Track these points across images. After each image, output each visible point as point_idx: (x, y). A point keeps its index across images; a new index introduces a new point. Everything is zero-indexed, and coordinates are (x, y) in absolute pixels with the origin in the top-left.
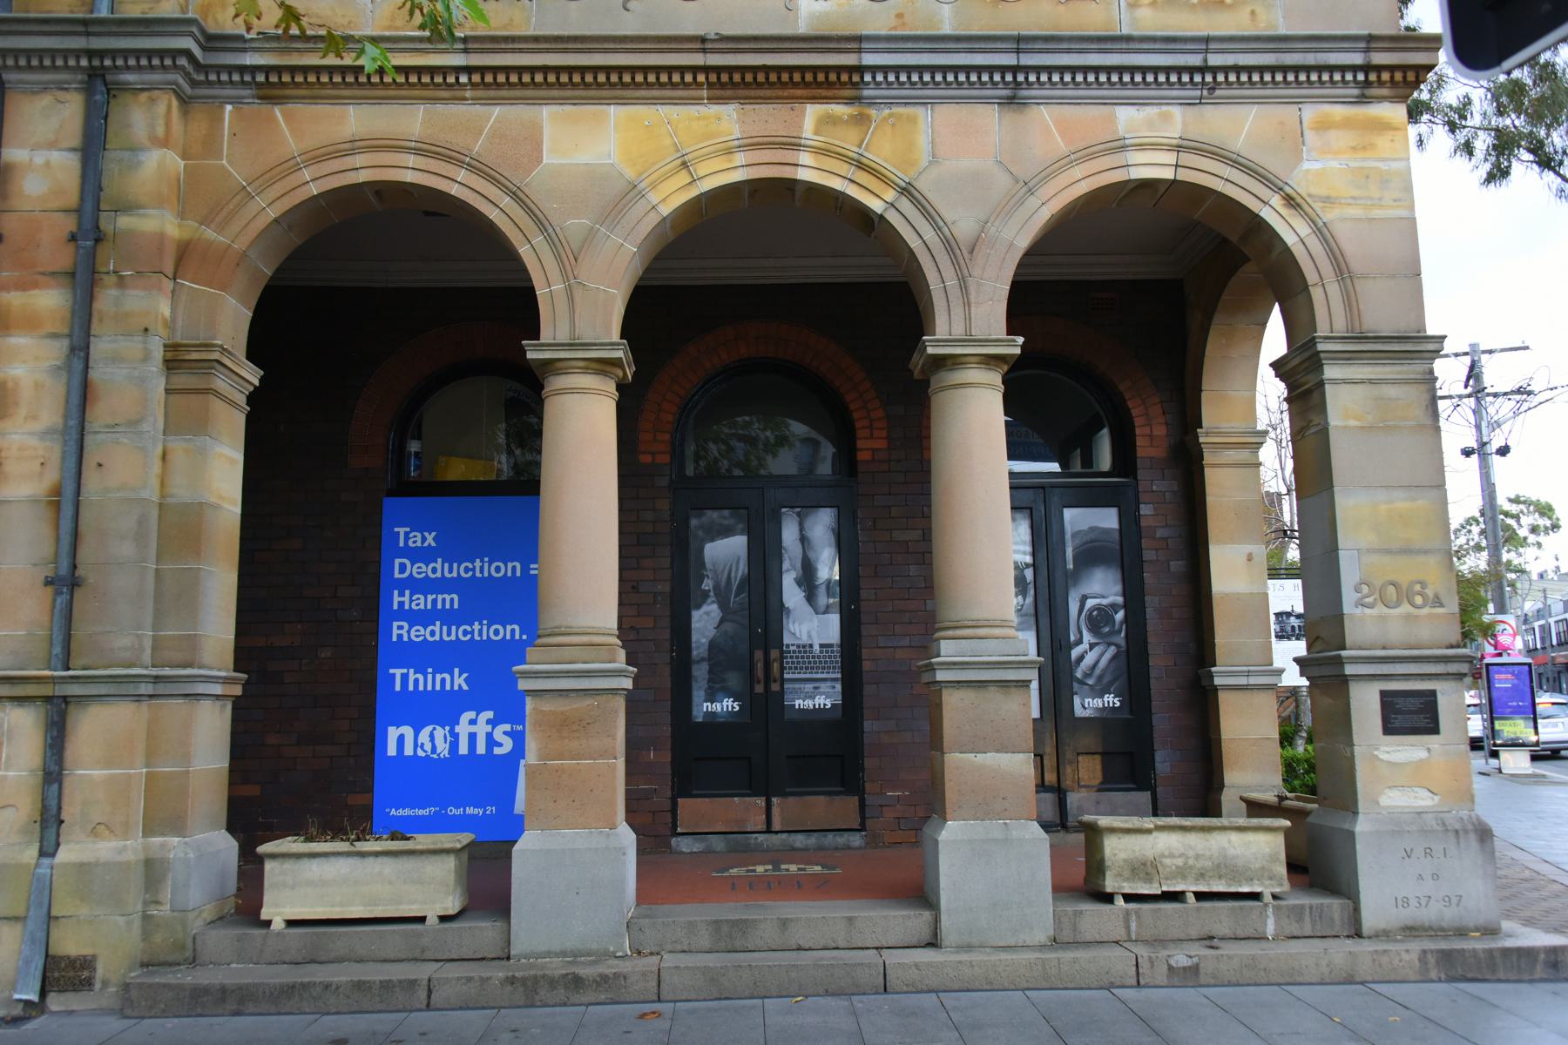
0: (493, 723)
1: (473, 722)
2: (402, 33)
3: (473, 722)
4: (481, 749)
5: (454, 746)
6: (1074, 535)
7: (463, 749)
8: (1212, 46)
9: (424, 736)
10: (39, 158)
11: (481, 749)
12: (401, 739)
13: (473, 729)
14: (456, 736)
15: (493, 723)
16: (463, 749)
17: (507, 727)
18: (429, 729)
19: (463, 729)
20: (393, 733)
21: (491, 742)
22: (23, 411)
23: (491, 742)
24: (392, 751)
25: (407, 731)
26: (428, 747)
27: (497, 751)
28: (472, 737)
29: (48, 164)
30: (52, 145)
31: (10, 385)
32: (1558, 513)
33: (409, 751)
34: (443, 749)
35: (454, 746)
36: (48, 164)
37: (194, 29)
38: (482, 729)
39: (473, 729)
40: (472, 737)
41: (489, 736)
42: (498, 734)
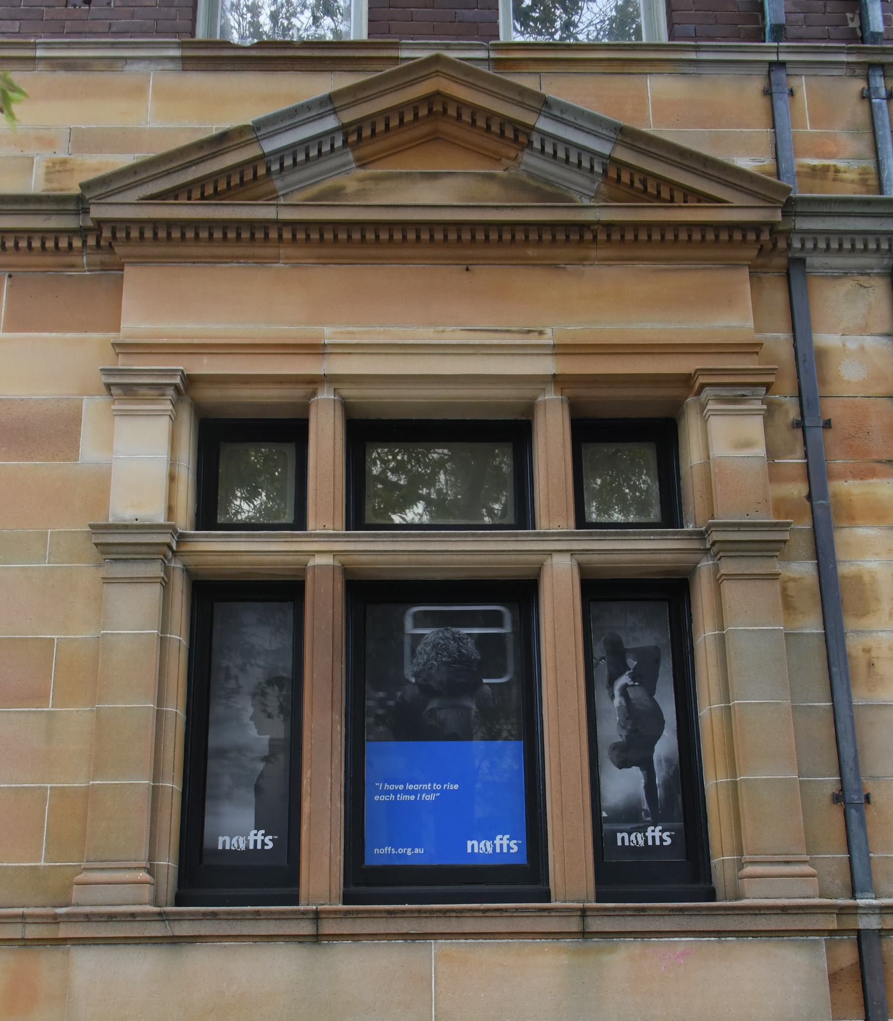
1: (501, 839)
4: (259, 847)
6: (660, 761)
7: (498, 850)
9: (234, 841)
10: (852, 343)
11: (259, 847)
12: (473, 846)
13: (501, 842)
14: (495, 845)
15: (264, 835)
17: (271, 837)
18: (236, 838)
19: (497, 842)
21: (509, 847)
22: (885, 606)
23: (509, 847)
25: (475, 842)
26: (484, 849)
27: (511, 851)
29: (862, 348)
30: (863, 330)
31: (866, 579)
33: (476, 851)
35: (494, 849)
36: (862, 348)
39: (501, 842)
40: (501, 845)
41: (263, 841)
42: (267, 840)
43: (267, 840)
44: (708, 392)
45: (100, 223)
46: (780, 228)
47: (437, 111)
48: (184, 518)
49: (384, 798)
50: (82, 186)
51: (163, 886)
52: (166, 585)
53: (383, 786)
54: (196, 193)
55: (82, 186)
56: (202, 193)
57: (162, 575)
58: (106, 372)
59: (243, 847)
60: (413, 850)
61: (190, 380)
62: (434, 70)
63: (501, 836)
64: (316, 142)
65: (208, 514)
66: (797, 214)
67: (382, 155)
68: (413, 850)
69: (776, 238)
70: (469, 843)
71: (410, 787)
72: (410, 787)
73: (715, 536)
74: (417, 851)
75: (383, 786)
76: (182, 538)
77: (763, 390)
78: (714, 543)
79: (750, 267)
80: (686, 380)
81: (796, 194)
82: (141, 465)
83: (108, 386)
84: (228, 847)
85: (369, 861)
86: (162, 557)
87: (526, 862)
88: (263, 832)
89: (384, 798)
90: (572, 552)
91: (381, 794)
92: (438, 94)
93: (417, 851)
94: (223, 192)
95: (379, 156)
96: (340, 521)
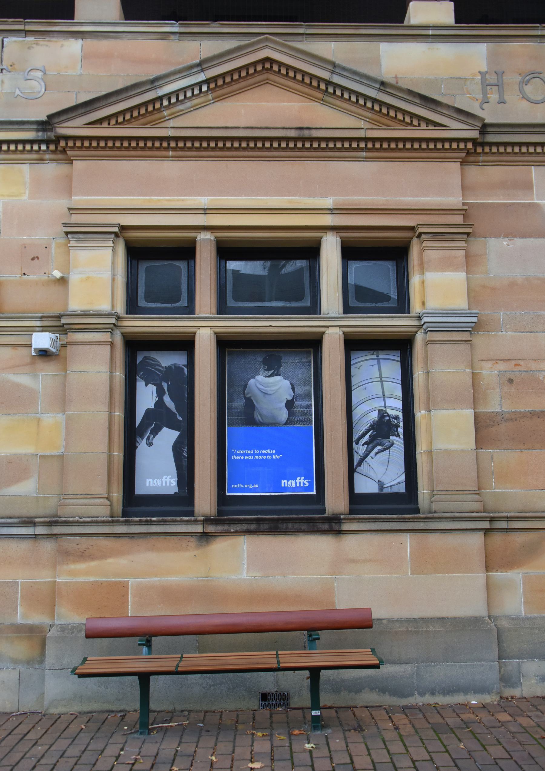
0: (171, 478)
1: (166, 478)
2: (9, 315)
3: (166, 478)
4: (168, 485)
5: (162, 484)
7: (164, 484)
8: (337, 70)
11: (168, 485)
12: (150, 482)
15: (171, 478)
16: (164, 484)
19: (298, 481)
20: (148, 481)
21: (304, 484)
23: (304, 484)
24: (147, 485)
27: (305, 486)
28: (166, 482)
32: (35, 256)
33: (286, 486)
34: (159, 484)
35: (162, 484)
37: (429, 329)
38: (302, 481)
40: (166, 482)
41: (170, 481)
43: (306, 482)
44: (423, 236)
45: (59, 138)
46: (478, 141)
47: (267, 68)
48: (120, 308)
49: (238, 458)
50: (48, 117)
51: (115, 504)
52: (112, 344)
53: (236, 452)
54: (113, 122)
55: (48, 117)
56: (117, 121)
57: (111, 340)
58: (65, 225)
59: (294, 485)
60: (253, 485)
61: (123, 228)
62: (265, 45)
63: (166, 476)
64: (167, 97)
65: (132, 307)
66: (488, 133)
67: (199, 106)
68: (253, 485)
69: (485, 144)
70: (283, 482)
71: (263, 452)
72: (263, 452)
73: (425, 319)
74: (255, 486)
75: (236, 452)
76: (118, 318)
77: (465, 236)
78: (425, 323)
79: (461, 162)
80: (412, 229)
81: (488, 120)
82: (96, 279)
83: (67, 233)
84: (151, 485)
85: (140, 490)
86: (110, 330)
87: (405, 491)
88: (303, 478)
89: (238, 458)
90: (340, 326)
91: (237, 455)
92: (267, 59)
93: (255, 486)
94: (128, 120)
95: (275, 84)
96: (214, 310)
